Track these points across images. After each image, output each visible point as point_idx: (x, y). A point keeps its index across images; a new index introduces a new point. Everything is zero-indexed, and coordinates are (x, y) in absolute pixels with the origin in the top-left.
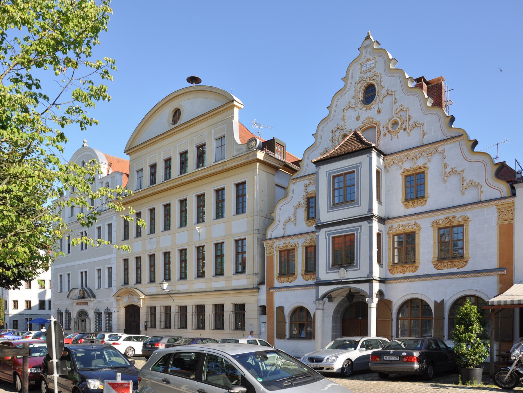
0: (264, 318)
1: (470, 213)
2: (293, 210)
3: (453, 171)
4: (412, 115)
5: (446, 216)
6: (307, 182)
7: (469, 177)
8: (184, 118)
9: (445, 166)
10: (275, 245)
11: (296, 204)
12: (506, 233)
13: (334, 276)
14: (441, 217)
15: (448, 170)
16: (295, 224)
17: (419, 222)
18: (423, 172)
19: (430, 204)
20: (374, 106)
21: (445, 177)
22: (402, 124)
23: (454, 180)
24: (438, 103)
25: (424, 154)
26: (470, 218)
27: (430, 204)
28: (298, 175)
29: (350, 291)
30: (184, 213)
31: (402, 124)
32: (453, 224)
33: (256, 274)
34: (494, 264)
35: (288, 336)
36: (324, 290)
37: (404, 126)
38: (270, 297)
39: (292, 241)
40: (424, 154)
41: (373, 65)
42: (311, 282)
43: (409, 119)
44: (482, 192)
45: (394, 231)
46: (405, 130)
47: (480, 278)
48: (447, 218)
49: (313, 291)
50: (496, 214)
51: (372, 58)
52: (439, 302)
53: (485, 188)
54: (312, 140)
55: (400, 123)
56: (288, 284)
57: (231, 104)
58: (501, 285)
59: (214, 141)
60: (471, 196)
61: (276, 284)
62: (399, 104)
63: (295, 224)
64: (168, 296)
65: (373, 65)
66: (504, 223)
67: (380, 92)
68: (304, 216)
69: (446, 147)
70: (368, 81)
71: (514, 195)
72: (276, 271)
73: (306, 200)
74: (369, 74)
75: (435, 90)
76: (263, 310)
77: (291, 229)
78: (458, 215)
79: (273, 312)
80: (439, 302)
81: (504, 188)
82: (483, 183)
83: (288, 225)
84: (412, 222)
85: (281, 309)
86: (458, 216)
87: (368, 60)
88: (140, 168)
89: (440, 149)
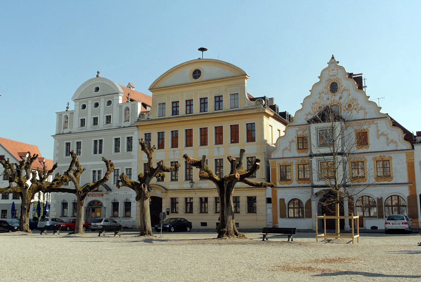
0: (270, 205)
1: (392, 155)
2: (289, 144)
3: (382, 134)
4: (359, 103)
5: (380, 155)
6: (298, 129)
7: (391, 137)
8: (203, 77)
9: (378, 131)
10: (277, 162)
11: (291, 140)
12: (411, 166)
13: (322, 183)
14: (378, 155)
15: (380, 133)
16: (290, 152)
17: (365, 157)
18: (366, 132)
19: (371, 148)
20: (338, 95)
21: (378, 136)
22: (354, 107)
23: (383, 138)
24: (361, 87)
25: (366, 123)
26: (393, 157)
27: (371, 148)
28: (292, 124)
29: (330, 191)
30: (188, 135)
31: (354, 107)
32: (384, 159)
33: (264, 179)
34: (406, 180)
35: (287, 217)
36: (316, 190)
37: (355, 107)
38: (274, 193)
39: (288, 161)
40: (366, 123)
41: (336, 73)
42: (310, 185)
43: (358, 105)
44: (398, 146)
45: (352, 160)
46: (355, 109)
47: (394, 187)
48: (381, 156)
49: (310, 190)
50: (405, 157)
51: (335, 69)
52: (379, 198)
53: (399, 144)
54: (301, 107)
55: (353, 106)
56: (287, 185)
57: (245, 76)
58: (410, 191)
59: (229, 95)
60: (392, 147)
61: (278, 184)
62: (352, 96)
63: (290, 152)
64: (193, 190)
65: (336, 73)
66: (409, 161)
67: (340, 88)
68: (296, 147)
69: (379, 121)
70: (333, 80)
71: (413, 148)
72: (278, 177)
73: (297, 138)
74: (334, 77)
75: (359, 80)
76: (269, 200)
77: (287, 154)
78: (387, 156)
79: (276, 202)
80: (379, 198)
81: (408, 145)
82: (398, 141)
83: (285, 151)
84: (362, 157)
85: (282, 200)
86: (386, 156)
87: (333, 70)
88: (163, 102)
89: (375, 122)
